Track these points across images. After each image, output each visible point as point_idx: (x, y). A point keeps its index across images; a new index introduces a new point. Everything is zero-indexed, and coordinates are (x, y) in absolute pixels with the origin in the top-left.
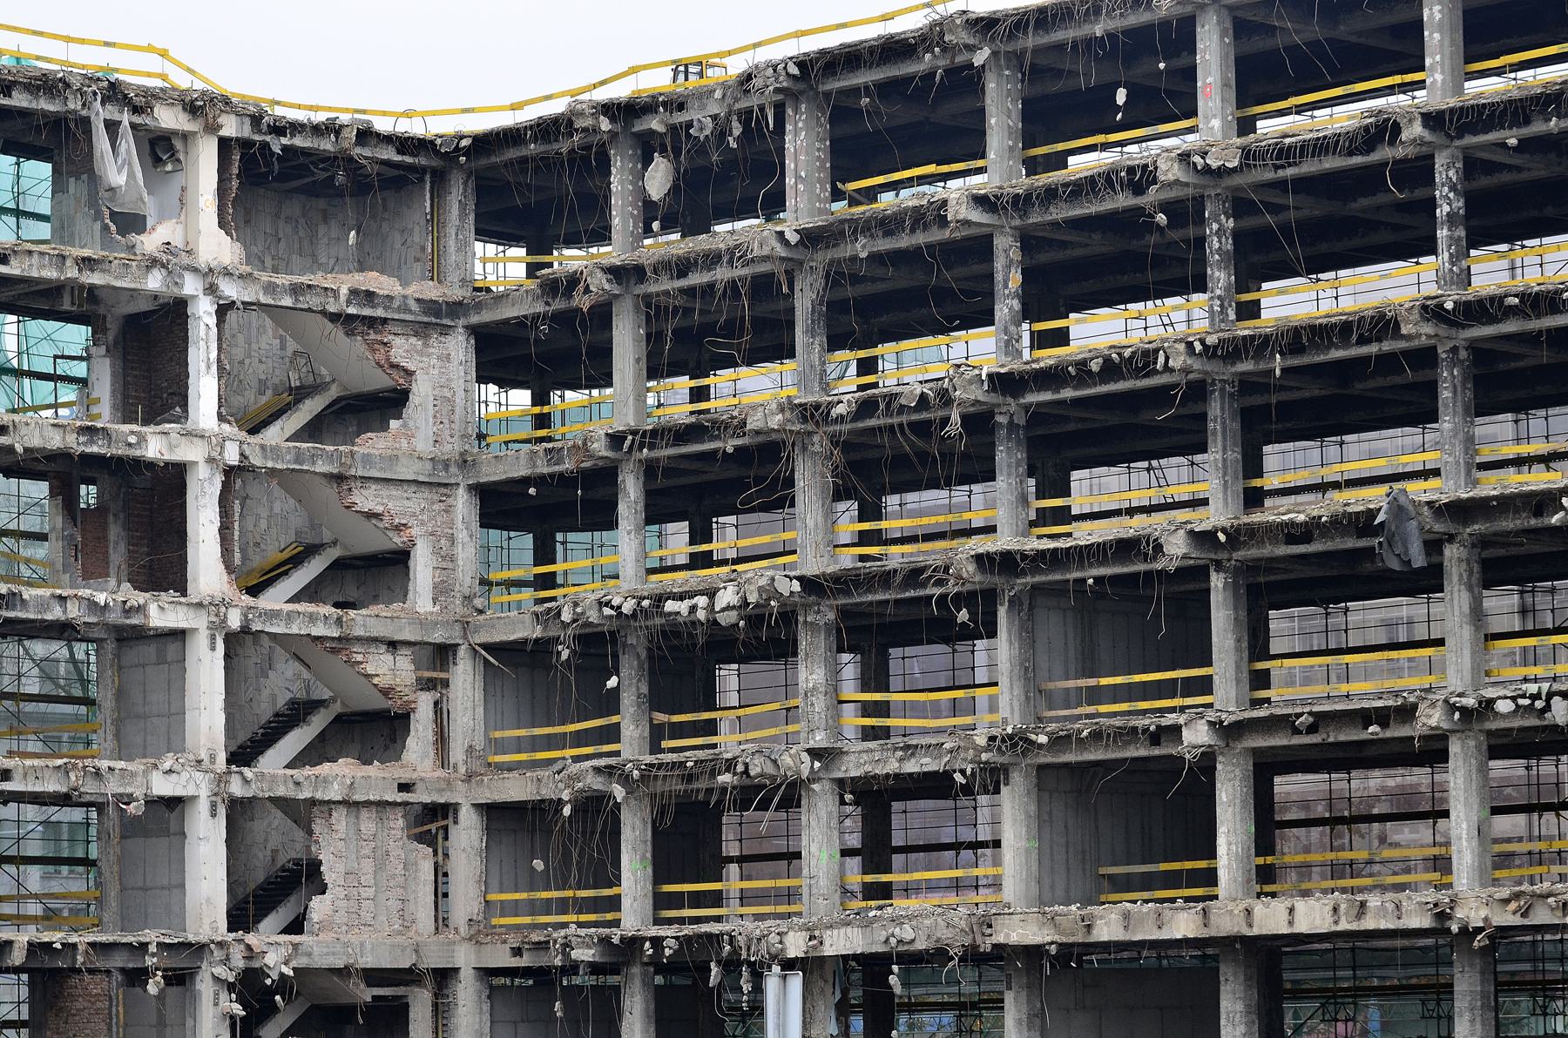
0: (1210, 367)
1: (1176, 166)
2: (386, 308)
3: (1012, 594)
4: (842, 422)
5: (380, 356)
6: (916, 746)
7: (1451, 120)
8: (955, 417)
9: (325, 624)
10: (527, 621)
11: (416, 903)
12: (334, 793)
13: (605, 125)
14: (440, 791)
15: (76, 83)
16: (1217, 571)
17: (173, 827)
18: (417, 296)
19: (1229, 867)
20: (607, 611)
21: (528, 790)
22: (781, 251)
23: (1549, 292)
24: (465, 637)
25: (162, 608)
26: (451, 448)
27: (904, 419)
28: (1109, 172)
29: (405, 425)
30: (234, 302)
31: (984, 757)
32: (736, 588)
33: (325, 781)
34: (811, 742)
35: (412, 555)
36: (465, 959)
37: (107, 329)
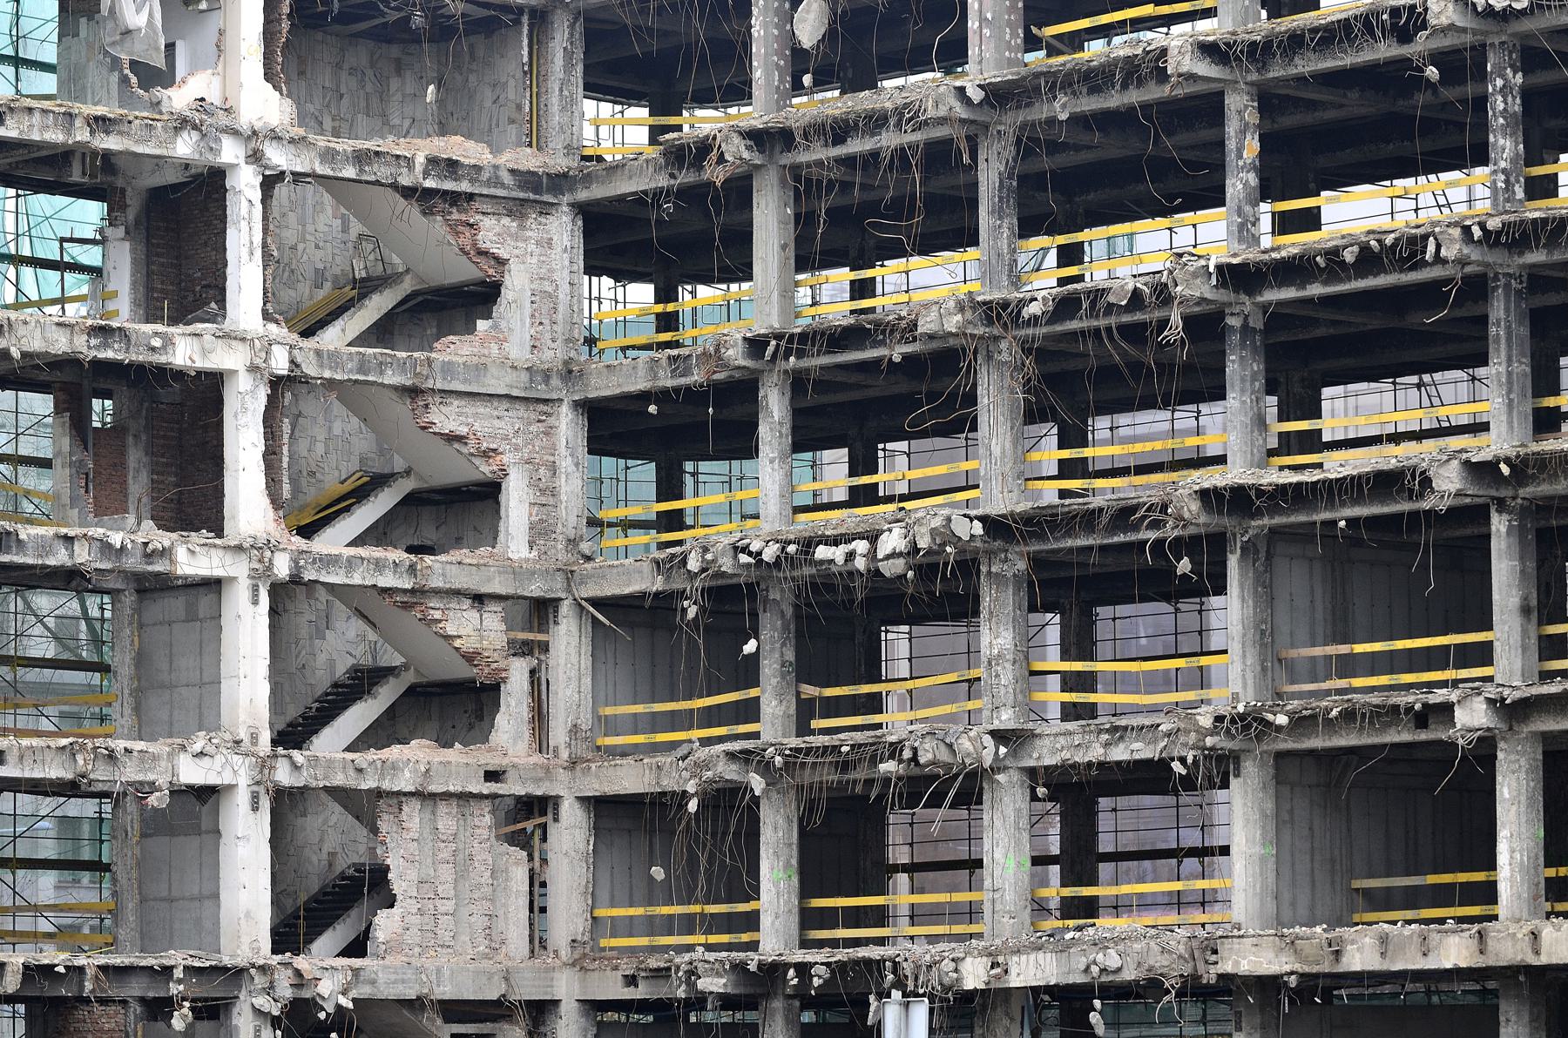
0: (1494, 257)
4: (1035, 325)
5: (465, 240)
6: (1126, 728)
8: (1176, 318)
9: (395, 572)
11: (506, 918)
12: (405, 782)
14: (537, 780)
16: (1499, 512)
18: (511, 165)
21: (646, 780)
22: (961, 111)
24: (569, 590)
25: (192, 552)
26: (553, 355)
27: (1112, 321)
28: (1367, 15)
30: (283, 173)
31: (1209, 741)
32: (904, 531)
33: (394, 768)
34: (996, 722)
37: (126, 206)
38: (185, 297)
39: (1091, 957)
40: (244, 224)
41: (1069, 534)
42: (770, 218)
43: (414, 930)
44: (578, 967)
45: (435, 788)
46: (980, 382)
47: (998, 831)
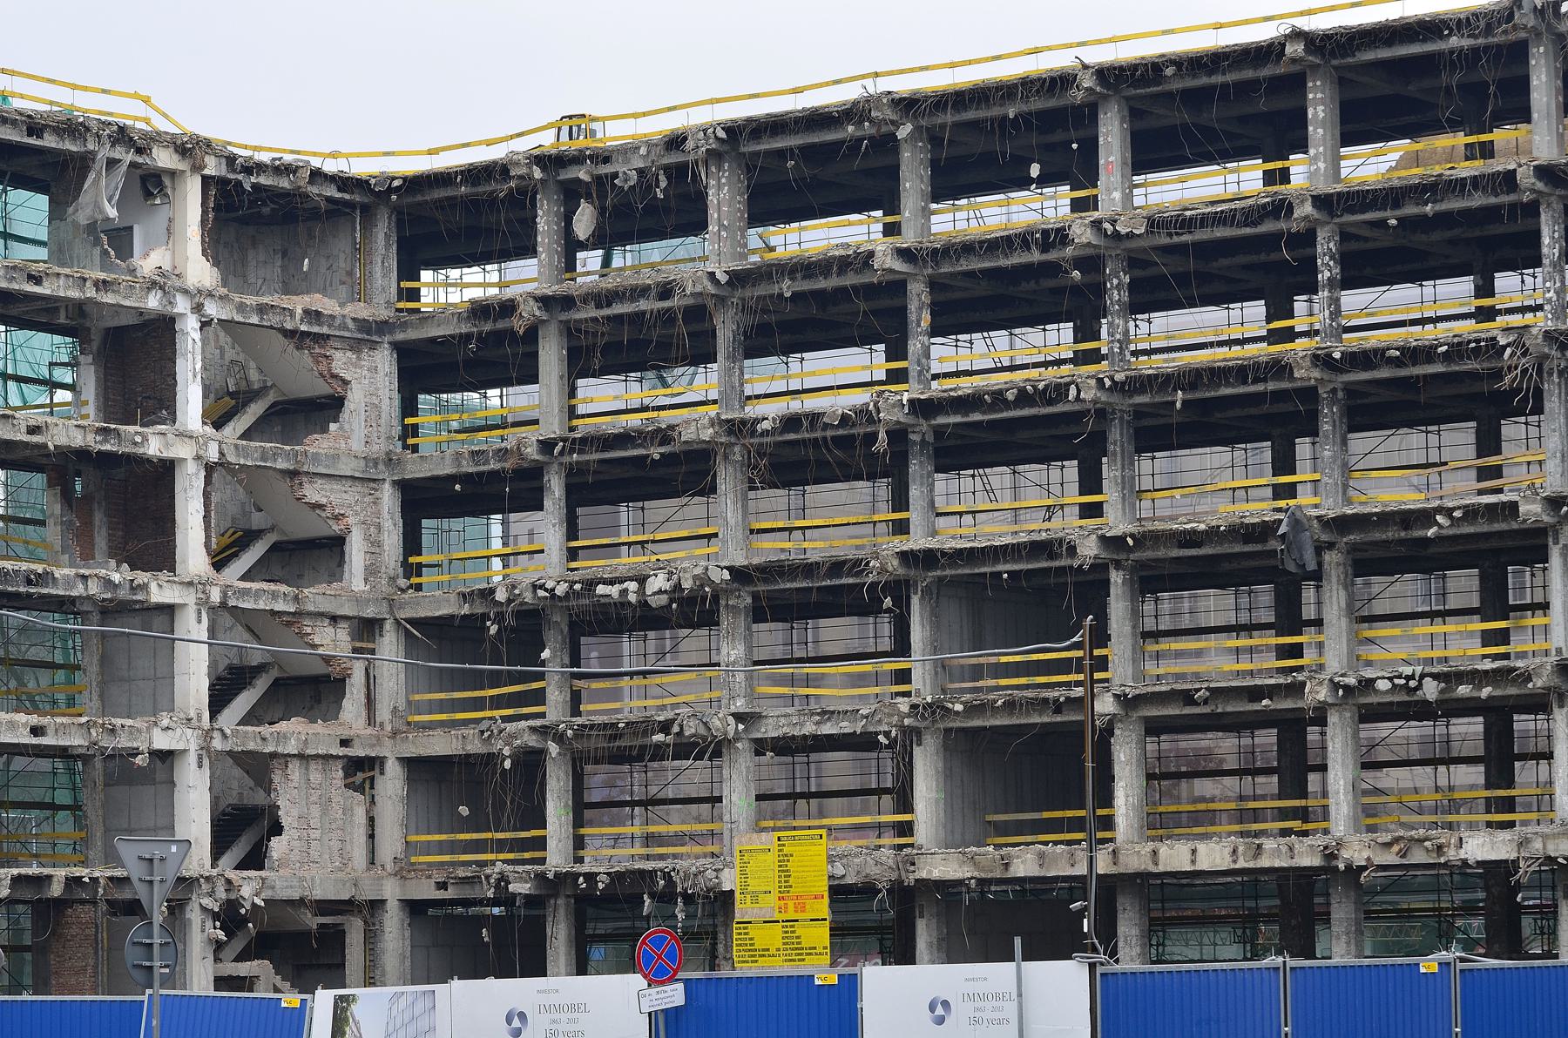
0: (1115, 398)
1: (1089, 230)
2: (330, 326)
4: (767, 436)
5: (323, 368)
6: (833, 712)
7: (1338, 203)
8: (882, 435)
9: (284, 600)
10: (452, 600)
11: (352, 842)
12: (291, 748)
13: (538, 174)
15: (94, 127)
16: (1117, 569)
17: (160, 775)
18: (353, 315)
19: (1127, 815)
20: (541, 593)
21: (454, 746)
22: (711, 289)
23: (1425, 347)
24: (391, 612)
25: (160, 586)
26: (379, 448)
27: (829, 433)
29: (341, 428)
30: (212, 320)
31: (907, 722)
33: (281, 737)
34: (733, 707)
36: (391, 892)
37: (91, 340)
38: (129, 405)
40: (190, 355)
42: (552, 357)
44: (399, 877)
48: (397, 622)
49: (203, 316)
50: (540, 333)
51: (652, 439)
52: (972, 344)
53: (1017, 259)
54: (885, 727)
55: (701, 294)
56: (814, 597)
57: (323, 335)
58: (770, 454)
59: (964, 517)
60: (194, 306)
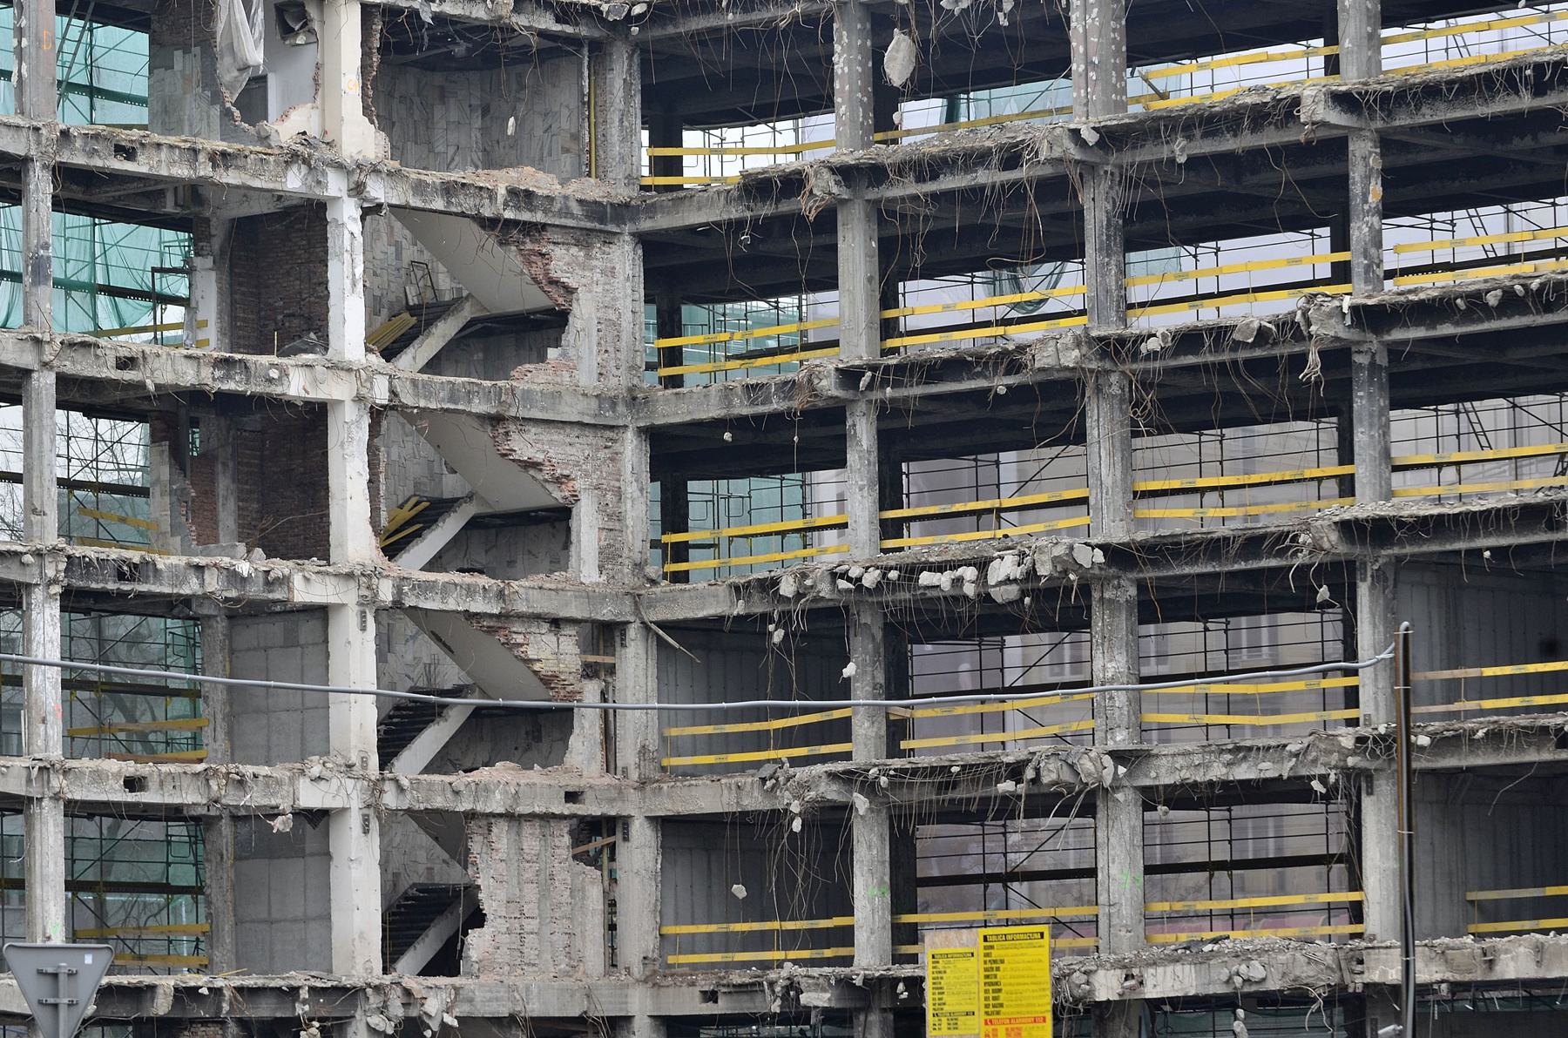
2: (545, 212)
3: (1376, 567)
4: (1155, 359)
5: (537, 270)
6: (1250, 749)
8: (1313, 358)
9: (484, 597)
10: (722, 595)
12: (496, 804)
14: (611, 801)
17: (311, 845)
18: (579, 196)
20: (843, 584)
22: (1075, 153)
24: (637, 612)
25: (307, 580)
26: (617, 382)
27: (1242, 355)
28: (1510, 70)
29: (564, 355)
30: (380, 206)
31: (1351, 761)
32: (1017, 558)
33: (482, 790)
34: (1110, 743)
35: (574, 512)
38: (265, 326)
39: (1234, 969)
40: (347, 256)
41: (1194, 562)
43: (504, 949)
44: (650, 984)
45: (523, 809)
46: (1089, 414)
47: (1114, 848)
48: (645, 626)
49: (365, 200)
50: (839, 217)
51: (996, 365)
52: (1454, 225)
53: (1502, 105)
54: (1322, 768)
55: (1060, 160)
56: (1222, 586)
57: (535, 224)
58: (1159, 385)
59: (1325, 483)
60: (352, 186)
